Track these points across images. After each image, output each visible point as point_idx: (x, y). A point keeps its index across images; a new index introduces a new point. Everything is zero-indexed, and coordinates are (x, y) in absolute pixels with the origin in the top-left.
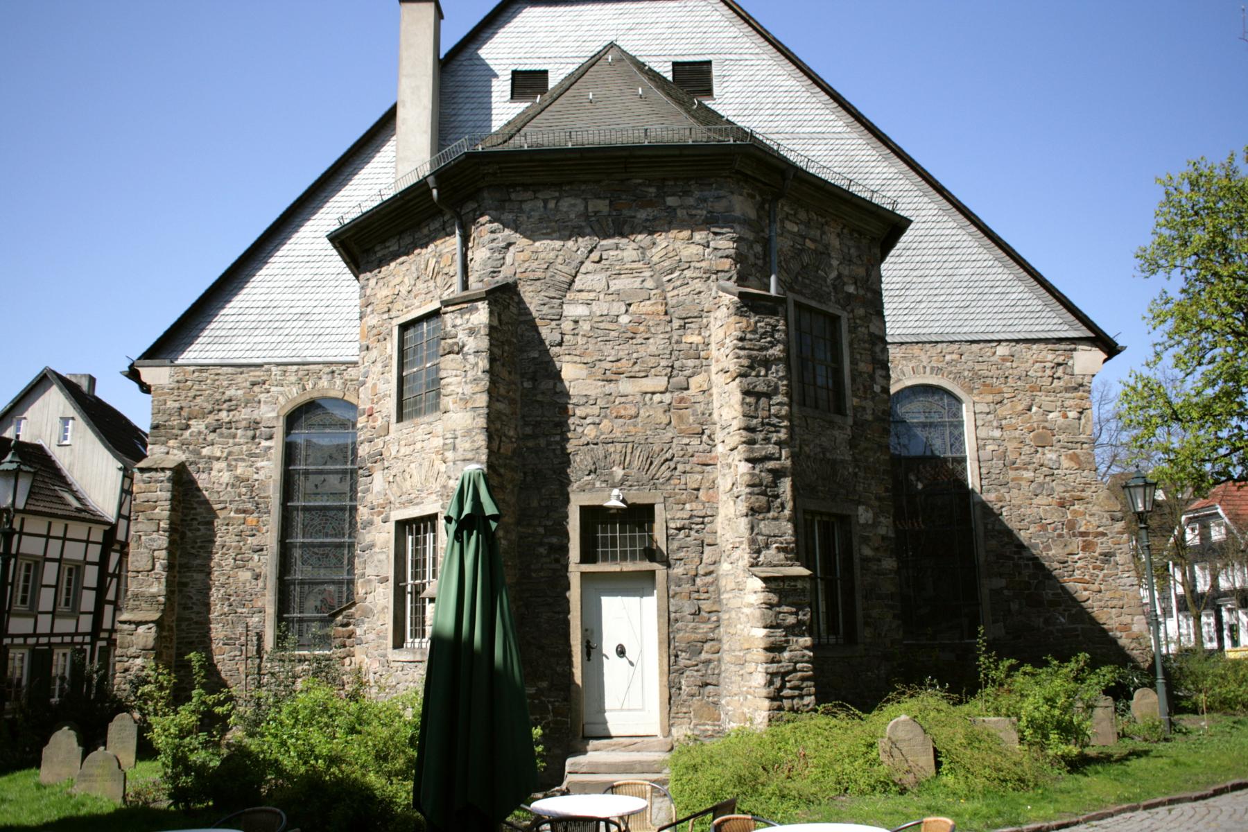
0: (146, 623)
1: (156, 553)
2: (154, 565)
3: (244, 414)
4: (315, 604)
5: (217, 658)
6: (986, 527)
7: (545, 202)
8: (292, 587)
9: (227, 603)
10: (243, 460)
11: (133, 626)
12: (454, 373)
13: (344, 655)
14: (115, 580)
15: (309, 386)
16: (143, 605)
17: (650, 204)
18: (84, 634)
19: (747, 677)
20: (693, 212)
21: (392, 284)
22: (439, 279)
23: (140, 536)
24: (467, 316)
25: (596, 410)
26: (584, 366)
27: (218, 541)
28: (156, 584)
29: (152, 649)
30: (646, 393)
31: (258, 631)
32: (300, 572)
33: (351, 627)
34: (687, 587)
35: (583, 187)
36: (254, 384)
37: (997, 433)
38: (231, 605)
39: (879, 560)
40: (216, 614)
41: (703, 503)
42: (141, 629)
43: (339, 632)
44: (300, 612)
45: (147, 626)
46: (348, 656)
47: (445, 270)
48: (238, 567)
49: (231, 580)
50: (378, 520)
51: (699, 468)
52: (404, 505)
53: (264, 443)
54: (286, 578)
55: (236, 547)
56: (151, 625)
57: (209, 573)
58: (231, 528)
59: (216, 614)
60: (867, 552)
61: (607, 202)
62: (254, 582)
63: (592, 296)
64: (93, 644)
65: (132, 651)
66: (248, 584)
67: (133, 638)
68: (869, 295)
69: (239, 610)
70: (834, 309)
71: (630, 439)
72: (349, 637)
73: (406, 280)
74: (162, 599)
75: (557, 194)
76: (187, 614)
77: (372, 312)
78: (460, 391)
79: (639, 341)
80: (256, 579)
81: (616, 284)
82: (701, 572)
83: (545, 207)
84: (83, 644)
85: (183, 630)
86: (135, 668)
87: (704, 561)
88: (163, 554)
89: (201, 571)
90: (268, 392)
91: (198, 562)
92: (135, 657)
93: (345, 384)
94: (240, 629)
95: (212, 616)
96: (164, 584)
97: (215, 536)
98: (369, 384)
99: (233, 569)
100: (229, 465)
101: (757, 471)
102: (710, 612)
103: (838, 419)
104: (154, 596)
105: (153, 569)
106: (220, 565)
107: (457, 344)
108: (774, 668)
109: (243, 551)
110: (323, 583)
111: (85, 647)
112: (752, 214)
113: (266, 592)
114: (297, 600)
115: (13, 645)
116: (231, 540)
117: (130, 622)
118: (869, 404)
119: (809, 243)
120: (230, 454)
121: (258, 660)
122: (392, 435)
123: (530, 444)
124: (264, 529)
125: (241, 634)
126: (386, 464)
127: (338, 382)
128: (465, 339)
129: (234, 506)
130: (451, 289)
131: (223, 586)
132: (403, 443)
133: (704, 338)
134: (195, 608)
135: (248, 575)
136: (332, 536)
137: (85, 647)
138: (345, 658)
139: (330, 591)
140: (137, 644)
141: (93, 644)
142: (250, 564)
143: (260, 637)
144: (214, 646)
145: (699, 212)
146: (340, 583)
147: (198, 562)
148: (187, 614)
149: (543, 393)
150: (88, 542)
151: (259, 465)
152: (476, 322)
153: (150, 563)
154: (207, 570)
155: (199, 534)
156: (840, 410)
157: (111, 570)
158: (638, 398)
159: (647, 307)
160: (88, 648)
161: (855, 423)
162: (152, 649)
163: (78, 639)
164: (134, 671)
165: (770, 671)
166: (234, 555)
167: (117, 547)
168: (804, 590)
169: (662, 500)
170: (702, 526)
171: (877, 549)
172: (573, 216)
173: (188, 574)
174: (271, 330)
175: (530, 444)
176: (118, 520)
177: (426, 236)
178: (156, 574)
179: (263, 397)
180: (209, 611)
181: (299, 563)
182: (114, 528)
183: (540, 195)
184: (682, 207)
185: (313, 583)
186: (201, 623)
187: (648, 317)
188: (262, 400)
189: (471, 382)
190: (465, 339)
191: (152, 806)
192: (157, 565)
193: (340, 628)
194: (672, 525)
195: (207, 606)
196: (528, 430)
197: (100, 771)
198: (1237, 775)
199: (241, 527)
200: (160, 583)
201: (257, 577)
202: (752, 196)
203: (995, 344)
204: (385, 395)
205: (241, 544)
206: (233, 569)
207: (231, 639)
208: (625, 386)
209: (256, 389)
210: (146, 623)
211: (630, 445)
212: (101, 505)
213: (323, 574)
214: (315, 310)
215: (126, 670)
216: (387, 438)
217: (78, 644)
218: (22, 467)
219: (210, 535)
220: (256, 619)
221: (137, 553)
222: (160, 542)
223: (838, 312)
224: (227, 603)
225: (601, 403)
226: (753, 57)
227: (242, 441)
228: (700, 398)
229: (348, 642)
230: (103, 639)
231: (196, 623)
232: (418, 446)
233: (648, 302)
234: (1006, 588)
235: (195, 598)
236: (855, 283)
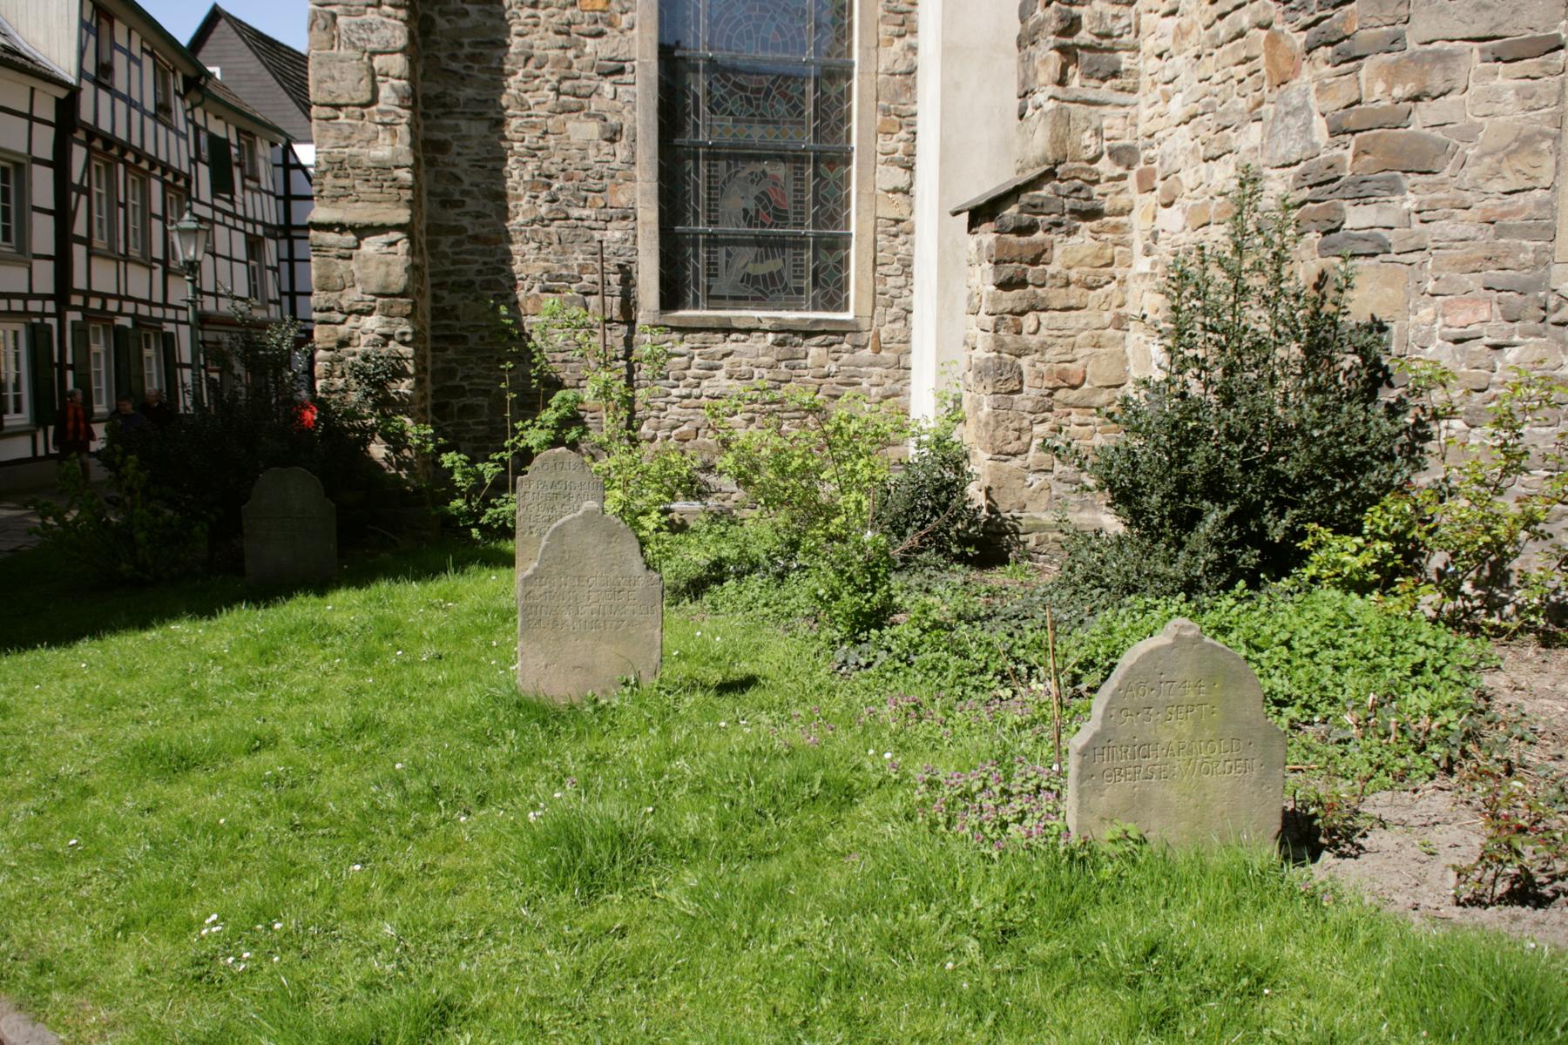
0: (382, 229)
1: (378, 62)
2: (375, 92)
4: (743, 204)
5: (527, 320)
8: (690, 164)
9: (544, 194)
11: (350, 238)
13: (1024, 305)
14: (83, 199)
16: (361, 187)
18: (44, 297)
23: (334, 16)
27: (515, 44)
28: (385, 136)
29: (403, 295)
31: (622, 261)
32: (706, 130)
33: (1039, 236)
38: (554, 201)
40: (520, 219)
42: (371, 245)
43: (1011, 246)
44: (710, 223)
45: (385, 238)
46: (1033, 308)
48: (567, 110)
49: (551, 141)
54: (677, 141)
55: (557, 63)
56: (394, 235)
57: (499, 123)
58: (542, 13)
59: (520, 219)
62: (606, 147)
64: (60, 315)
65: (351, 297)
66: (592, 152)
67: (353, 265)
69: (575, 212)
72: (1035, 262)
74: (405, 175)
76: (451, 216)
80: (612, 140)
84: (43, 315)
85: (445, 255)
86: (364, 339)
88: (398, 63)
89: (479, 116)
91: (469, 92)
92: (360, 313)
94: (578, 257)
95: (512, 225)
96: (407, 139)
97: (508, 32)
99: (553, 113)
104: (383, 167)
105: (374, 101)
106: (523, 105)
109: (575, 71)
110: (759, 158)
111: (48, 320)
113: (637, 171)
114: (703, 194)
116: (544, 42)
117: (342, 228)
121: (623, 330)
124: (624, 21)
125: (583, 268)
131: (532, 152)
134: (472, 206)
135: (592, 129)
136: (775, 48)
137: (48, 320)
138: (1023, 313)
139: (775, 177)
140: (364, 282)
141: (60, 315)
142: (594, 105)
143: (627, 276)
144: (521, 294)
146: (798, 159)
147: (469, 92)
148: (451, 216)
150: (31, 118)
153: (366, 83)
154: (492, 114)
155: (465, 23)
157: (76, 179)
160: (53, 322)
162: (403, 295)
163: (34, 306)
164: (362, 345)
166: (554, 79)
167: (81, 135)
173: (447, 122)
176: (80, 80)
178: (382, 113)
180: (504, 214)
181: (703, 108)
182: (74, 92)
185: (740, 155)
186: (486, 241)
192: (384, 91)
193: (1012, 238)
195: (499, 198)
197: (1184, 727)
199: (568, 13)
200: (394, 135)
201: (613, 136)
205: (571, 54)
206: (553, 113)
207: (559, 278)
210: (382, 229)
212: (43, 50)
213: (757, 134)
215: (343, 343)
217: (35, 314)
219: (495, 29)
220: (614, 234)
221: (331, 58)
222: (387, 33)
224: (544, 194)
229: (1031, 273)
230: (76, 308)
231: (475, 238)
235: (467, 181)
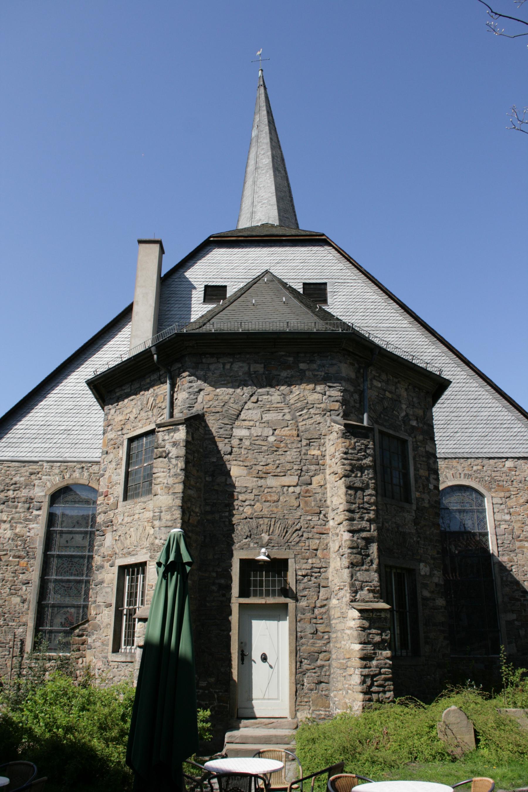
3: (24, 493)
6: (502, 579)
7: (224, 364)
10: (21, 523)
12: (162, 470)
15: (67, 476)
17: (289, 367)
19: (348, 677)
20: (316, 373)
21: (125, 413)
22: (155, 410)
24: (172, 434)
25: (252, 496)
30: (284, 486)
33: (84, 637)
34: (309, 615)
35: (248, 356)
36: (31, 474)
37: (507, 517)
39: (434, 600)
47: (159, 405)
50: (107, 565)
51: (317, 536)
52: (124, 555)
53: (36, 513)
60: (426, 594)
61: (262, 365)
63: (251, 423)
68: (425, 427)
70: (403, 435)
71: (273, 516)
73: (134, 410)
75: (231, 360)
77: (111, 430)
78: (165, 481)
79: (281, 453)
81: (267, 417)
82: (318, 605)
83: (224, 368)
87: (320, 598)
90: (41, 479)
93: (90, 475)
98: (106, 476)
100: (11, 526)
102: (323, 633)
103: (406, 505)
107: (165, 451)
112: (353, 375)
118: (426, 496)
119: (387, 394)
120: (12, 518)
122: (120, 509)
123: (209, 517)
126: (115, 528)
127: (86, 474)
128: (170, 448)
129: (12, 553)
130: (163, 417)
132: (126, 514)
133: (322, 452)
145: (320, 373)
149: (218, 484)
152: (177, 438)
158: (279, 489)
159: (286, 431)
161: (417, 509)
165: (364, 673)
169: (293, 556)
170: (319, 574)
171: (432, 592)
172: (240, 374)
174: (45, 440)
175: (209, 517)
177: (148, 383)
179: (37, 482)
183: (221, 360)
184: (308, 370)
187: (286, 438)
188: (36, 484)
189: (173, 476)
190: (170, 448)
194: (300, 573)
196: (208, 508)
202: (352, 364)
203: (504, 460)
204: (116, 483)
208: (271, 481)
209: (33, 477)
214: (74, 428)
216: (116, 511)
223: (406, 438)
225: (255, 492)
226: (352, 281)
227: (21, 510)
228: (319, 490)
232: (136, 517)
234: (517, 620)
236: (417, 420)
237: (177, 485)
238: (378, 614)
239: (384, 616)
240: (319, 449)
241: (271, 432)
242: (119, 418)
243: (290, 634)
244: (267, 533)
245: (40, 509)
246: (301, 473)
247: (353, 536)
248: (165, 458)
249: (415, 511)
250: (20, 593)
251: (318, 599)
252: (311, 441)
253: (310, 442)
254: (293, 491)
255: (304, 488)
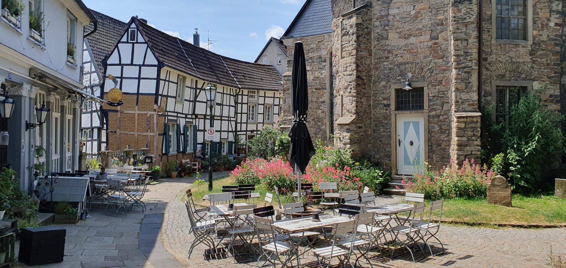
12: (346, 42)
26: (397, 33)
36: (319, 42)
41: (444, 86)
53: (324, 64)
63: (400, 4)
71: (415, 62)
87: (444, 109)
90: (324, 44)
101: (460, 73)
102: (445, 130)
103: (522, 43)
108: (461, 153)
115: (257, 134)
116: (314, 99)
129: (314, 87)
151: (322, 72)
156: (525, 38)
161: (534, 43)
165: (459, 154)
168: (477, 122)
169: (427, 85)
170: (443, 95)
174: (324, 20)
179: (322, 46)
187: (421, 10)
188: (322, 47)
191: (96, 217)
194: (431, 95)
198: (516, 218)
209: (320, 44)
211: (415, 64)
218: (212, 88)
227: (316, 64)
228: (443, 42)
233: (422, 4)
237: (353, 50)
238: (471, 119)
239: (476, 120)
240: (443, 15)
241: (412, 8)
242: (337, 9)
243: (425, 131)
244: (411, 73)
245: (325, 61)
246: (431, 32)
247: (459, 71)
248: (347, 35)
249: (531, 45)
250: (321, 108)
251: (442, 110)
252: (438, 10)
253: (437, 11)
254: (426, 44)
255: (434, 41)
